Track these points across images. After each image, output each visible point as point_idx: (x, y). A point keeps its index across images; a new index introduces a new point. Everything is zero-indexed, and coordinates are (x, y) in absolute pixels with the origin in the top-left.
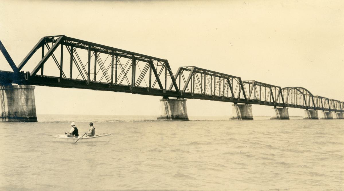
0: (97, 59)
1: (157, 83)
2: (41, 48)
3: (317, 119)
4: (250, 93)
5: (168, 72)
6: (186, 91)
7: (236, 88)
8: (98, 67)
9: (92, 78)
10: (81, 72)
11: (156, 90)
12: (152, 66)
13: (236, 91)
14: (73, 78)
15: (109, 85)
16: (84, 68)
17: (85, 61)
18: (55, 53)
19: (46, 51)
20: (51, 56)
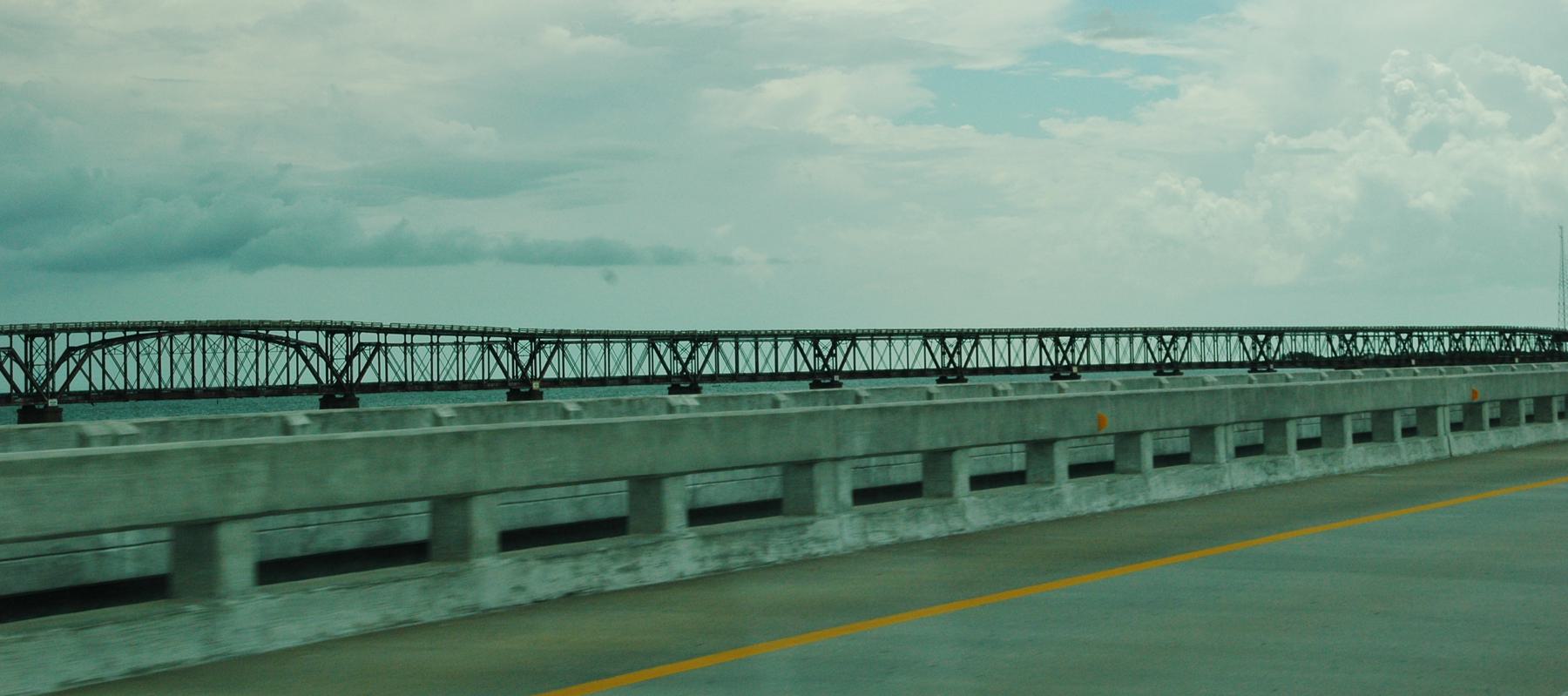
0: (538, 355)
1: (805, 364)
2: (66, 363)
3: (1323, 417)
4: (1521, 345)
5: (491, 353)
6: (1183, 361)
7: (1139, 351)
8: (415, 368)
9: (410, 379)
10: (396, 373)
11: (804, 373)
12: (926, 344)
13: (468, 371)
14: (857, 369)
15: (193, 392)
16: (400, 368)
17: (427, 361)
18: (546, 360)
19: (73, 365)
20: (370, 367)
